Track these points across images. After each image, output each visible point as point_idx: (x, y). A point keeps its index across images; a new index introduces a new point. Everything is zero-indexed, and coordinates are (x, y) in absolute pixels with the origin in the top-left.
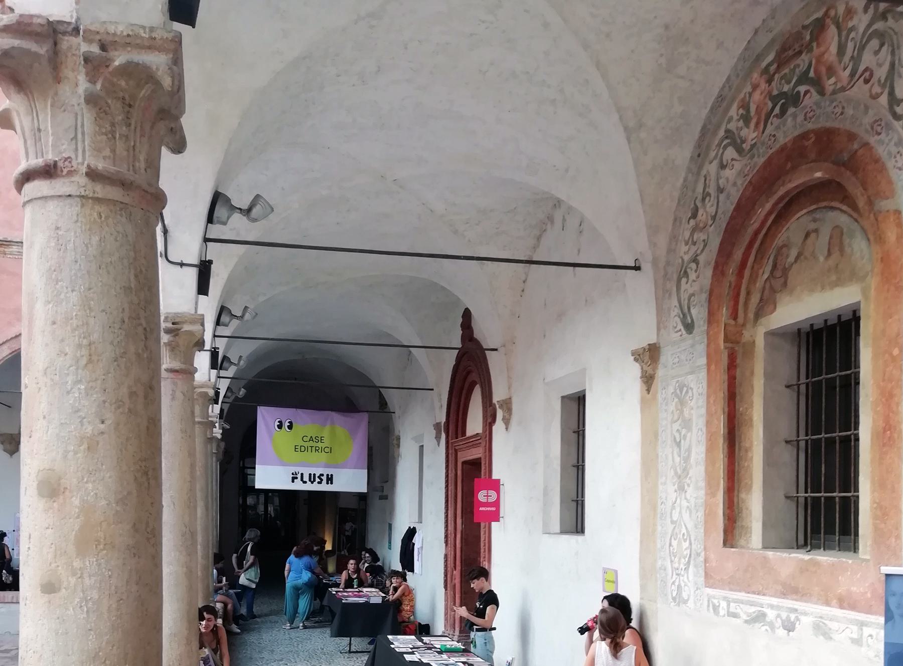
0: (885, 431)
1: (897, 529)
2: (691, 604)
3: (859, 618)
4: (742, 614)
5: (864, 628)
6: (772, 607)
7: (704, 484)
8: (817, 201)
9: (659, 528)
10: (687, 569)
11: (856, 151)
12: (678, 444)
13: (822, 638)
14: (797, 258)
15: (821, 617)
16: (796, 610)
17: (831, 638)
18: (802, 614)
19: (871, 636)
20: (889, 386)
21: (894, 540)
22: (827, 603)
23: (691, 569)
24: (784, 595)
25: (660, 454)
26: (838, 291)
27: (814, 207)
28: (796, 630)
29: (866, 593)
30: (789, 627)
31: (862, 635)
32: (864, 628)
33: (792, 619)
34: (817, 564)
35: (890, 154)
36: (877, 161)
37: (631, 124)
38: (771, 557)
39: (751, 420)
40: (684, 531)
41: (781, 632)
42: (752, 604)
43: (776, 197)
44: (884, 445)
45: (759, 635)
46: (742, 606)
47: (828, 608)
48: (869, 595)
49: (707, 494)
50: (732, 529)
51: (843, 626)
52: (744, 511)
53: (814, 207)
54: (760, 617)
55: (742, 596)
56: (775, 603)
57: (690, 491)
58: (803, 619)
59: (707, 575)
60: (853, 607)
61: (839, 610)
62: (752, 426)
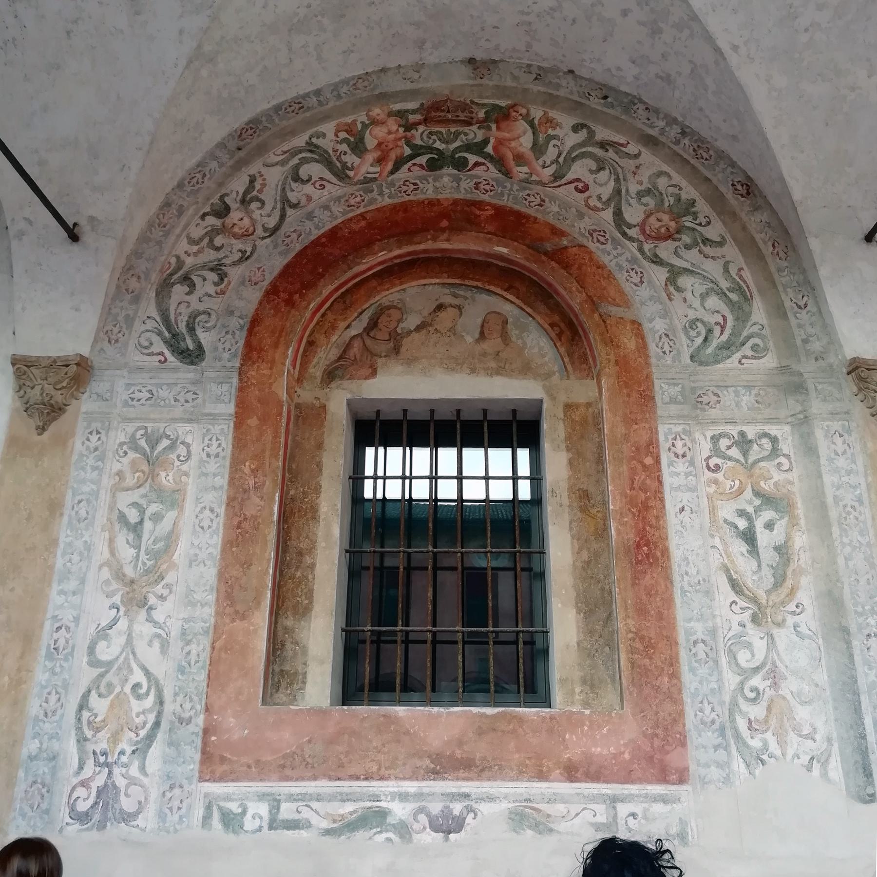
0: (638, 546)
1: (671, 665)
2: (147, 820)
3: (609, 792)
4: (315, 820)
5: (619, 806)
6: (403, 797)
7: (211, 598)
8: (463, 277)
9: (41, 676)
10: (141, 750)
11: (566, 248)
12: (136, 529)
13: (530, 833)
14: (418, 328)
15: (529, 800)
16: (467, 796)
17: (551, 830)
18: (481, 799)
19: (634, 815)
20: (643, 496)
21: (666, 679)
22: (541, 776)
23: (156, 751)
24: (435, 774)
25: (63, 540)
26: (498, 381)
27: (457, 281)
28: (467, 828)
29: (623, 753)
30: (448, 825)
31: (615, 816)
32: (619, 806)
33: (456, 812)
34: (520, 720)
35: (621, 267)
36: (600, 267)
37: (207, 48)
38: (401, 714)
39: (314, 510)
40: (138, 676)
41: (430, 838)
42: (345, 798)
43: (411, 248)
44: (639, 562)
45: (374, 849)
46: (315, 805)
47: (544, 785)
48: (627, 756)
49: (219, 614)
50: (280, 672)
51: (575, 808)
52: (289, 646)
53: (457, 281)
54: (374, 819)
55: (323, 786)
56: (412, 790)
57: (168, 611)
58: (484, 808)
59: (207, 756)
60: (596, 776)
61: (568, 785)
62: (315, 518)
